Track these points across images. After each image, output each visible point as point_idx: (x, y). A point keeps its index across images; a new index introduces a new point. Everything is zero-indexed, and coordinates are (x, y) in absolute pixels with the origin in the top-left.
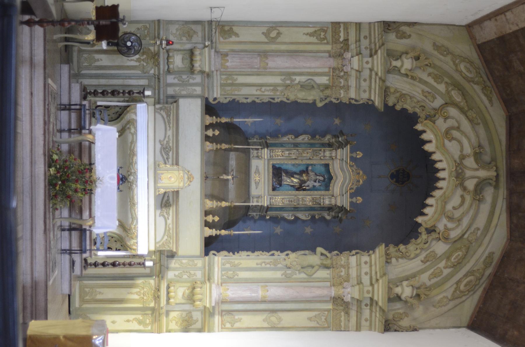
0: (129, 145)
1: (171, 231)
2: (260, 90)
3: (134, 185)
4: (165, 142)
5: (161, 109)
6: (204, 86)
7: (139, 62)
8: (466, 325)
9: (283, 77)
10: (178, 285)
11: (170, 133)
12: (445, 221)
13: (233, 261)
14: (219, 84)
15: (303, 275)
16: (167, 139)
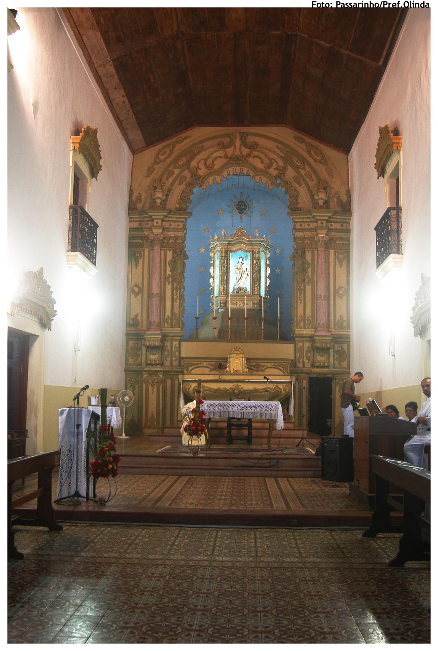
0: (212, 393)
1: (276, 364)
2: (176, 299)
3: (242, 390)
5: (187, 370)
6: (172, 339)
7: (154, 385)
8: (346, 156)
9: (167, 283)
10: (316, 361)
11: (205, 364)
13: (298, 320)
14: (171, 329)
15: (309, 270)
16: (209, 366)
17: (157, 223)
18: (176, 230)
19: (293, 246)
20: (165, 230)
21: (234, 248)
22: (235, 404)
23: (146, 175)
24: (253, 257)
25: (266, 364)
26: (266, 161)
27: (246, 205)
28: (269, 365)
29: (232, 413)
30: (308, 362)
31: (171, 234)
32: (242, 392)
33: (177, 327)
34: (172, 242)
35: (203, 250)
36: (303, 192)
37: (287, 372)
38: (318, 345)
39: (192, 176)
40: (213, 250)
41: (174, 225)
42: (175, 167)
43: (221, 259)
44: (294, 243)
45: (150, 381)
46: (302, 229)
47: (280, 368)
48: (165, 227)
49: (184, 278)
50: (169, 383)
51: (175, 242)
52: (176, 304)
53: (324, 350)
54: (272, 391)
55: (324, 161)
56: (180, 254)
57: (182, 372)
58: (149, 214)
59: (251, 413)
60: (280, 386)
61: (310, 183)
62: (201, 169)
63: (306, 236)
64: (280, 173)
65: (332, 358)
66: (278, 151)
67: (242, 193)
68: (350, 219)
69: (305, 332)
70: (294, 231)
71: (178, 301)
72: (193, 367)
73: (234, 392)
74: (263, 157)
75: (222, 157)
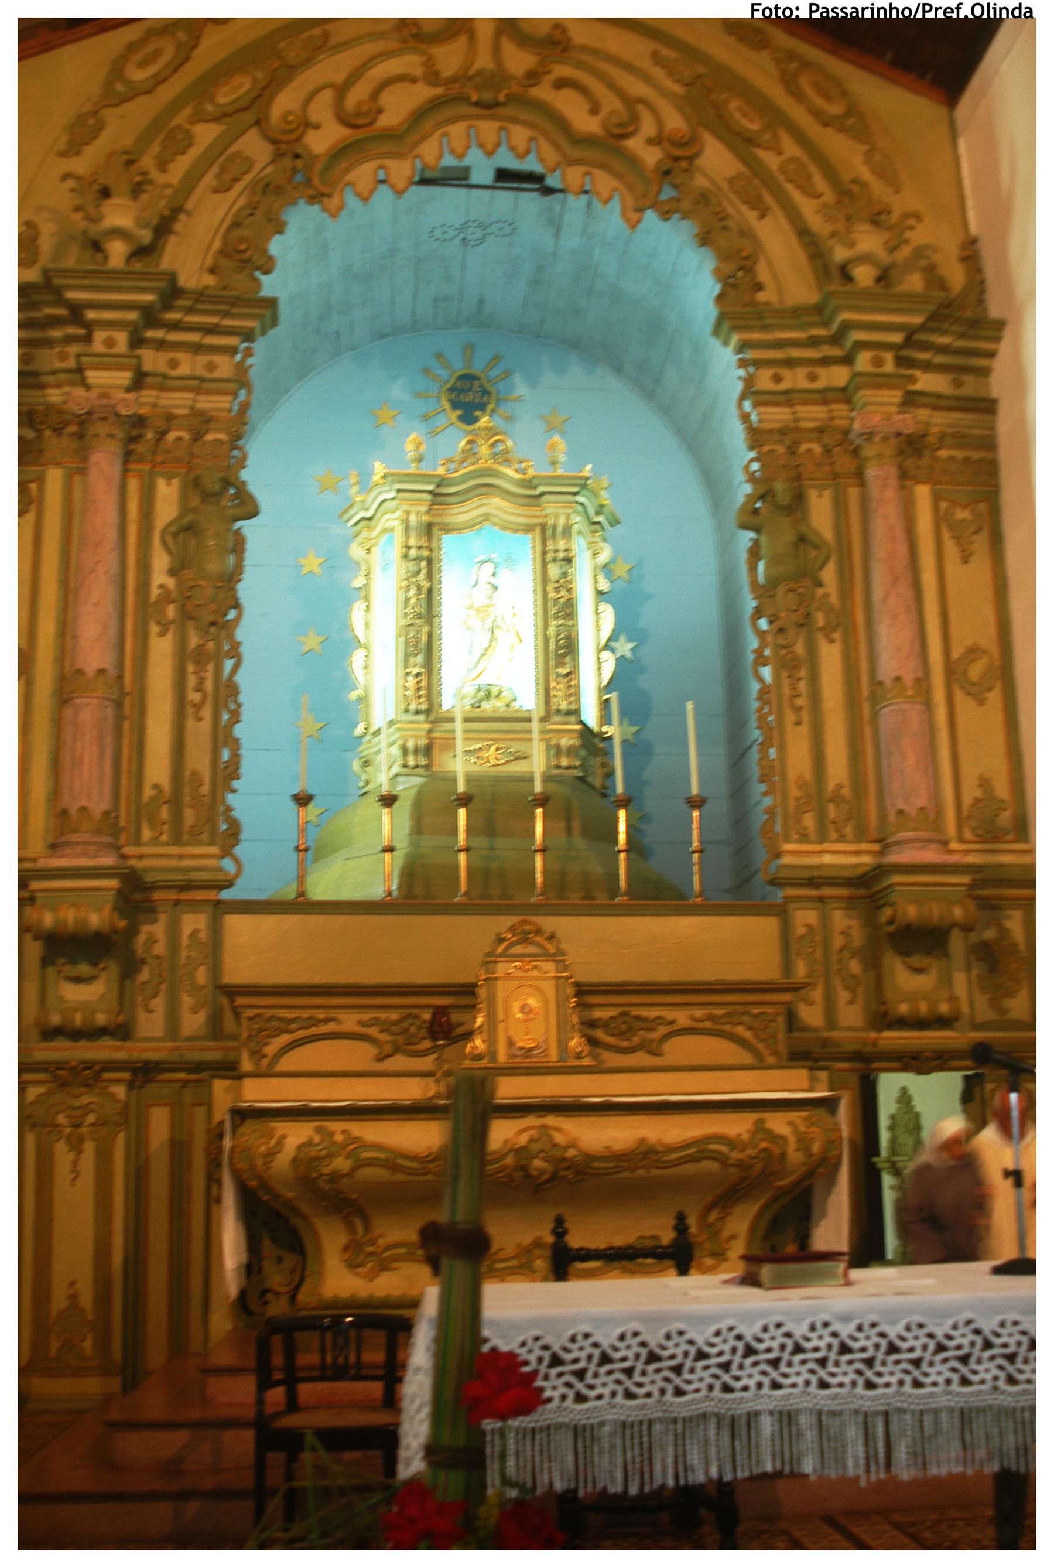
1: (719, 1012)
2: (198, 707)
3: (571, 1153)
4: (384, 1037)
5: (257, 1055)
6: (177, 903)
7: (82, 1140)
8: (941, 111)
9: (154, 629)
10: (889, 993)
11: (350, 1021)
12: (634, 144)
13: (792, 804)
14: (174, 850)
15: (829, 574)
16: (373, 1031)
17: (110, 343)
18: (200, 385)
19: (746, 468)
20: (150, 380)
21: (459, 514)
22: (800, 1330)
23: (61, 145)
24: (544, 553)
25: (669, 1014)
26: (611, 103)
27: (486, 392)
28: (682, 1017)
29: (767, 1424)
30: (851, 1002)
31: (179, 402)
32: (571, 1164)
33: (201, 843)
34: (179, 439)
35: (313, 563)
36: (775, 239)
37: (775, 1053)
38: (912, 912)
39: (278, 155)
40: (364, 534)
41: (187, 365)
42: (198, 118)
43: (405, 556)
44: (752, 454)
45: (61, 1119)
46: (786, 392)
47: (740, 1030)
48: (147, 367)
49: (237, 606)
50: (159, 1124)
51: (197, 437)
52: (199, 731)
53: (922, 940)
54: (735, 1155)
55: (854, 122)
56: (220, 500)
57: (229, 1069)
58: (72, 295)
59: (965, 1416)
60: (779, 1124)
61: (807, 207)
62: (317, 127)
63: (804, 424)
64: (677, 159)
65: (960, 979)
66: (659, 74)
67: (469, 349)
68: (991, 355)
69: (827, 859)
70: (747, 405)
71: (207, 713)
72: (285, 1039)
73: (524, 1168)
74: (599, 89)
75: (414, 80)
